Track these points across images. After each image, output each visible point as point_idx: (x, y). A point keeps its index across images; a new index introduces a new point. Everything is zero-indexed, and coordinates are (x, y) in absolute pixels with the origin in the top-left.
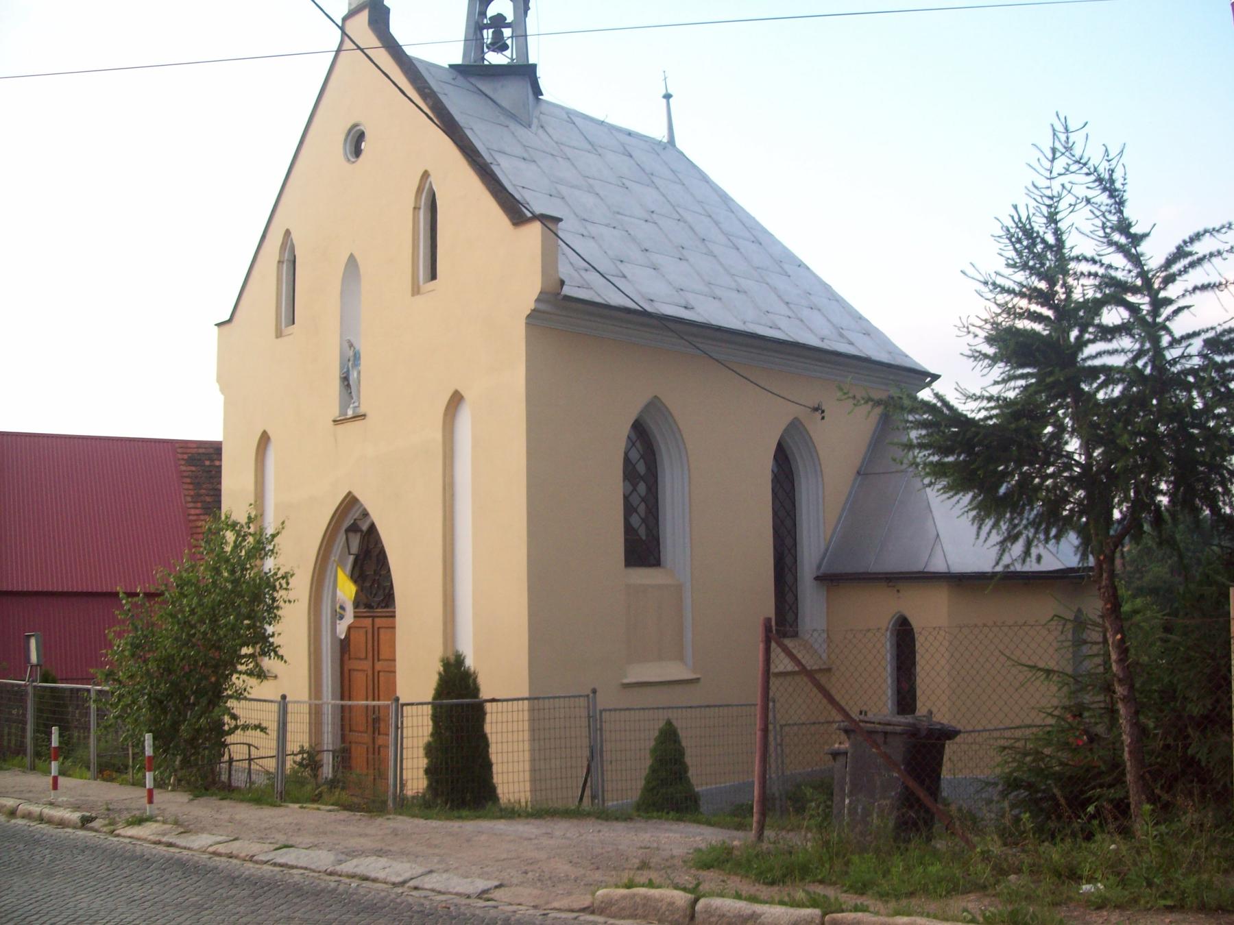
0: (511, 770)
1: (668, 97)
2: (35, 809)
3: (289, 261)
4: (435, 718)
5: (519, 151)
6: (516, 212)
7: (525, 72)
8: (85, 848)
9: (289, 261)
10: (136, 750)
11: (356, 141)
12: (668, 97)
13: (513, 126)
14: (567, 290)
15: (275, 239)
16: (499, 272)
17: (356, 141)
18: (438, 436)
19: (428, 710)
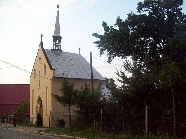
0: (46, 122)
1: (79, 49)
2: (3, 127)
3: (35, 71)
4: (37, 119)
5: (57, 59)
6: (51, 68)
7: (60, 50)
8: (6, 130)
9: (35, 71)
10: (121, 109)
11: (40, 59)
12: (79, 49)
13: (57, 56)
14: (56, 76)
15: (34, 69)
16: (50, 74)
17: (40, 59)
18: (45, 90)
19: (36, 118)
